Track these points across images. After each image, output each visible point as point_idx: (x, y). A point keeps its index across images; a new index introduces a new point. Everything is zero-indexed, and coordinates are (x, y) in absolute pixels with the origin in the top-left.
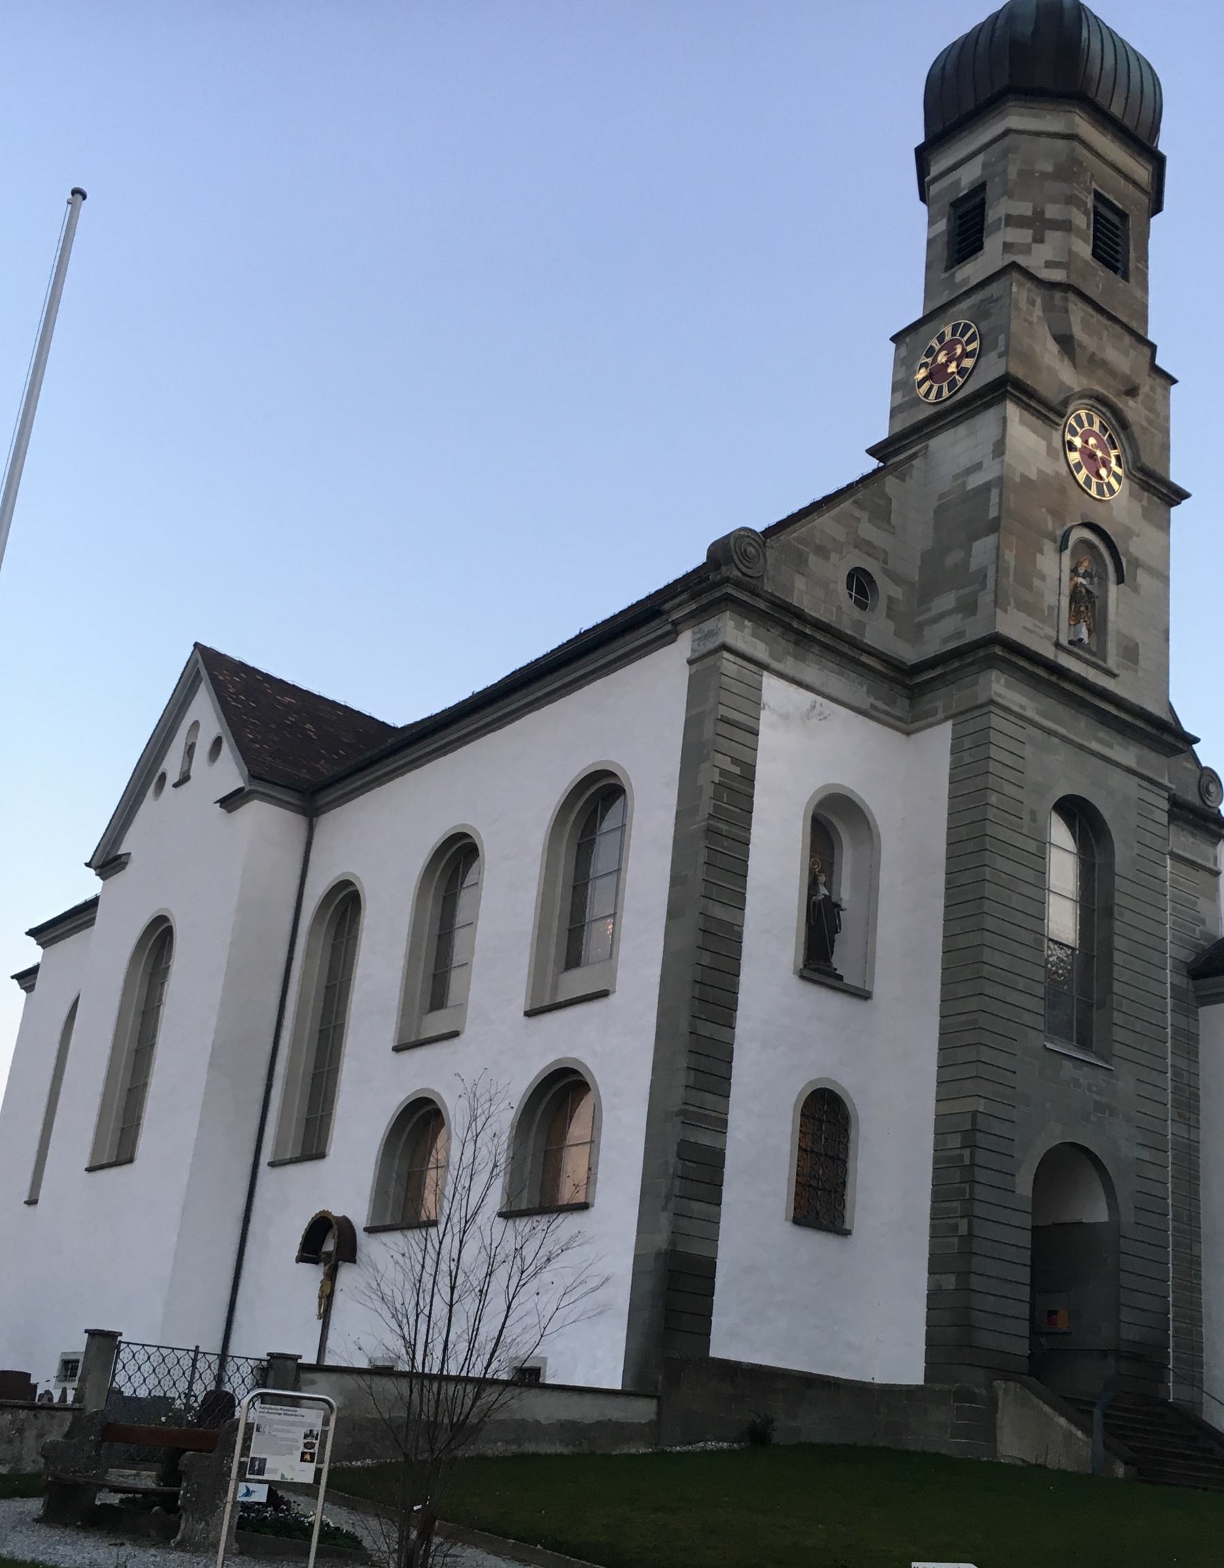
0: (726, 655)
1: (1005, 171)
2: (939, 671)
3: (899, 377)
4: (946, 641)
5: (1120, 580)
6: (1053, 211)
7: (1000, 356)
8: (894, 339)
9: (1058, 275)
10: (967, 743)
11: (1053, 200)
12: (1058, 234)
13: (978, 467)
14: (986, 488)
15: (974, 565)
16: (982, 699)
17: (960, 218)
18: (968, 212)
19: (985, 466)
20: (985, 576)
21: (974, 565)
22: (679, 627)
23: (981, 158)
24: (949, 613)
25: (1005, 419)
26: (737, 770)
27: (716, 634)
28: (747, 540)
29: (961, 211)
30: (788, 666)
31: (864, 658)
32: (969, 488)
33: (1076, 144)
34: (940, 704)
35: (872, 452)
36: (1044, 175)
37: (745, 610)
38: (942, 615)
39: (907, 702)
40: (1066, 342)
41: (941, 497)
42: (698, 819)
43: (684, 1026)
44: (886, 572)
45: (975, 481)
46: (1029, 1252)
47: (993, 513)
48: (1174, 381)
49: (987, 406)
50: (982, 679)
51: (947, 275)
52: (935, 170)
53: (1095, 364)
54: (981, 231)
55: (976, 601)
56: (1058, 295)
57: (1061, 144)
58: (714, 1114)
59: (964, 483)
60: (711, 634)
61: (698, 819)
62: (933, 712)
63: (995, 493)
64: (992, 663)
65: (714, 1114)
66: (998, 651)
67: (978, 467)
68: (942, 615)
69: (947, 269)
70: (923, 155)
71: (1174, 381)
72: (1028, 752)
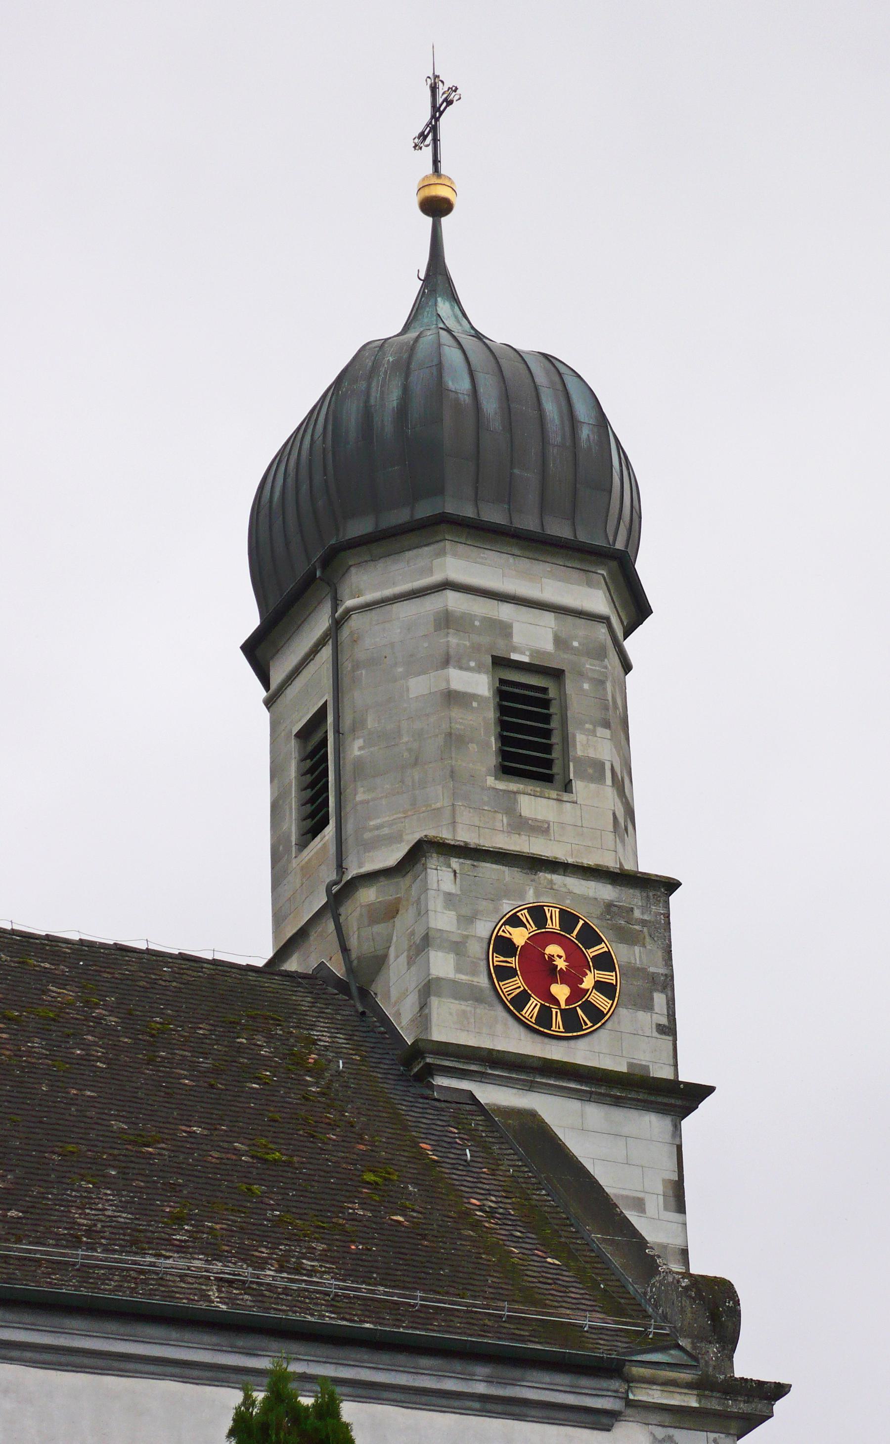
48: (672, 885)
52: (277, 677)
70: (258, 651)
71: (672, 885)
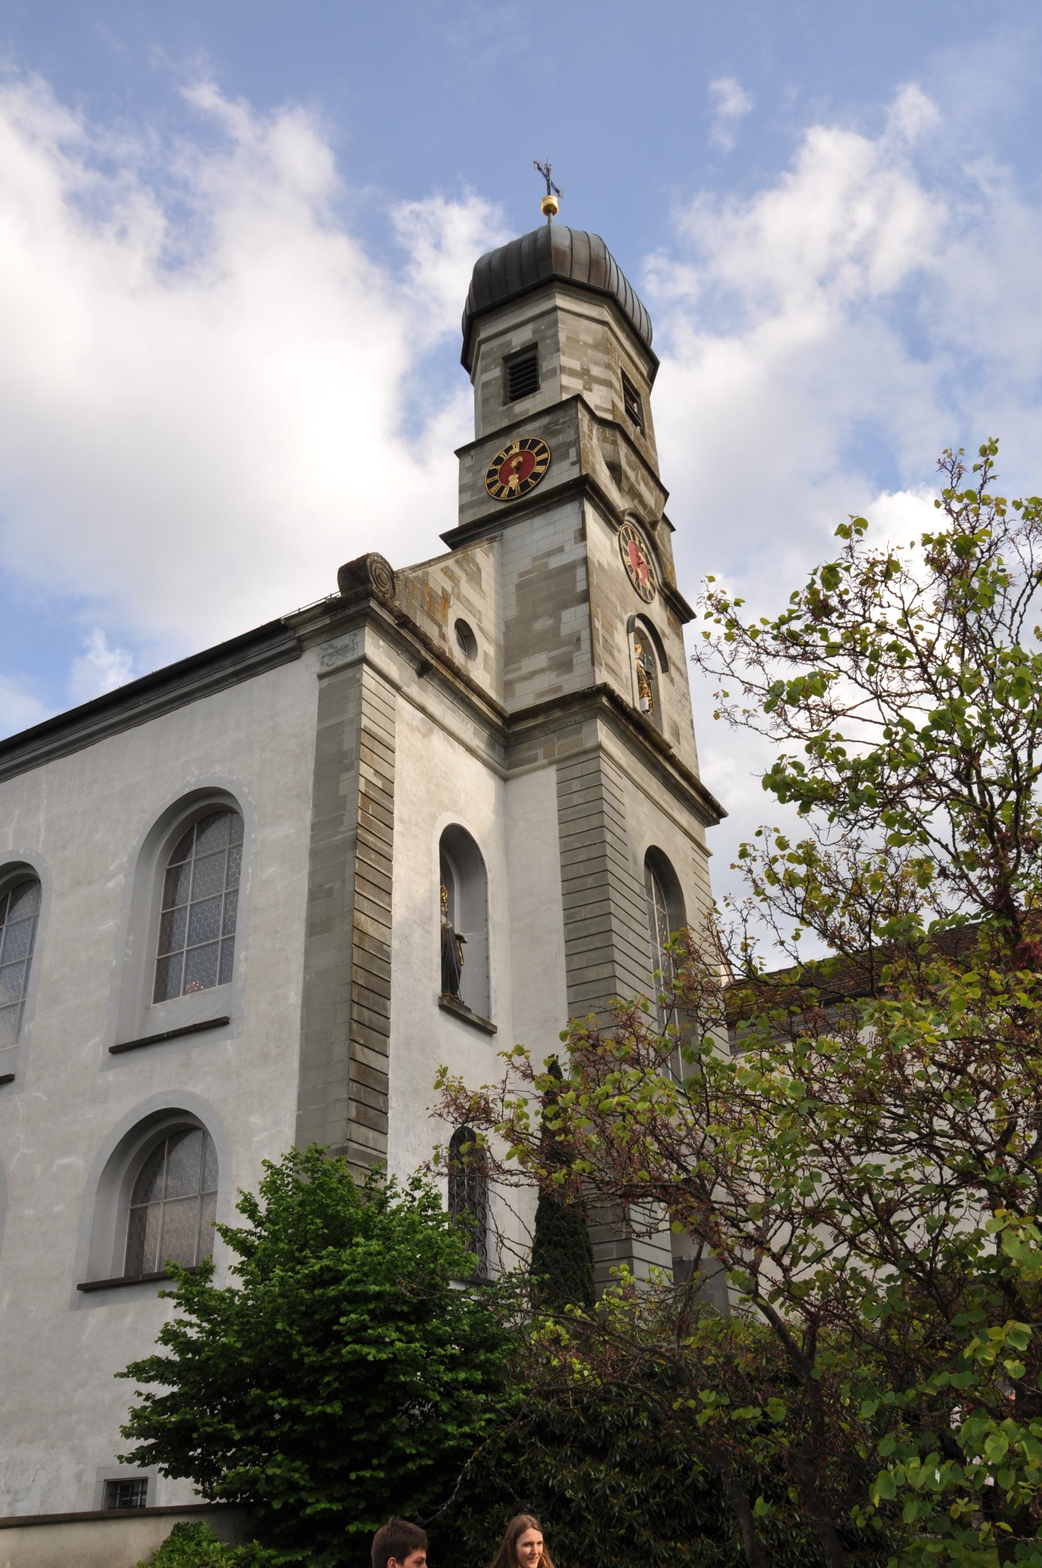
0: (365, 667)
1: (556, 335)
2: (540, 720)
3: (465, 481)
4: (540, 695)
5: (665, 669)
6: (596, 371)
7: (573, 464)
8: (460, 453)
9: (609, 417)
10: (576, 785)
11: (596, 363)
12: (602, 388)
13: (561, 550)
14: (571, 567)
15: (565, 630)
16: (589, 744)
17: (511, 368)
18: (518, 365)
19: (567, 548)
20: (579, 640)
21: (565, 630)
22: (305, 644)
23: (530, 327)
24: (543, 671)
25: (583, 513)
26: (379, 783)
27: (353, 649)
28: (380, 565)
29: (510, 364)
30: (413, 690)
31: (475, 700)
32: (551, 567)
33: (606, 328)
34: (541, 752)
35: (447, 537)
36: (586, 344)
37: (382, 629)
38: (534, 674)
39: (502, 750)
40: (614, 468)
41: (521, 575)
42: (342, 829)
43: (340, 1051)
44: (481, 629)
45: (555, 562)
46: (446, 1180)
47: (581, 587)
48: (673, 529)
49: (571, 499)
50: (585, 729)
51: (505, 408)
52: (483, 334)
53: (633, 493)
54: (536, 377)
55: (572, 660)
56: (608, 432)
57: (598, 327)
58: (375, 1153)
59: (546, 564)
60: (345, 649)
61: (342, 829)
62: (535, 759)
63: (580, 572)
64: (601, 712)
65: (375, 1153)
66: (604, 700)
67: (561, 550)
68: (534, 674)
69: (505, 404)
72: (625, 800)
